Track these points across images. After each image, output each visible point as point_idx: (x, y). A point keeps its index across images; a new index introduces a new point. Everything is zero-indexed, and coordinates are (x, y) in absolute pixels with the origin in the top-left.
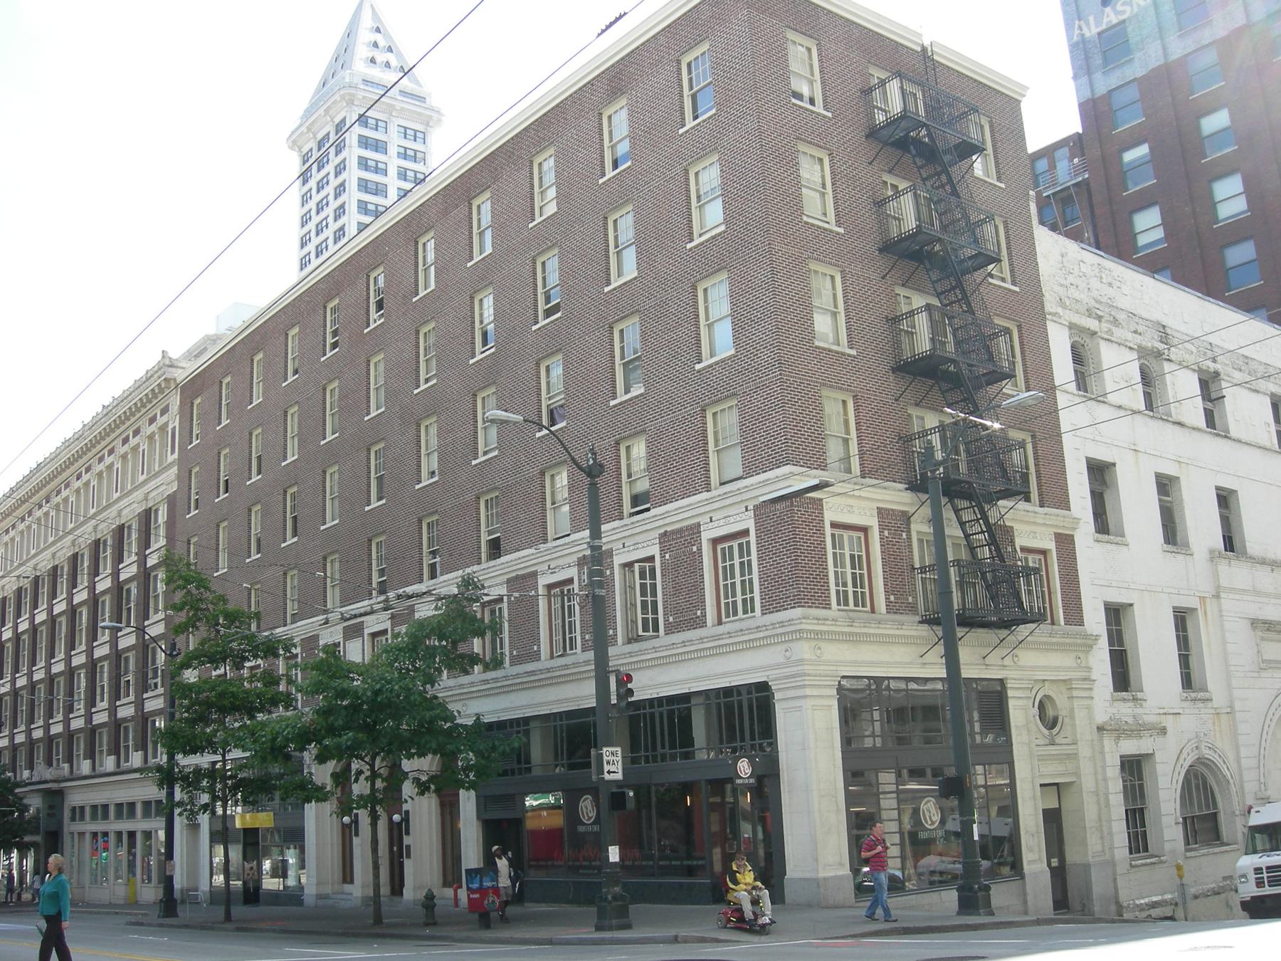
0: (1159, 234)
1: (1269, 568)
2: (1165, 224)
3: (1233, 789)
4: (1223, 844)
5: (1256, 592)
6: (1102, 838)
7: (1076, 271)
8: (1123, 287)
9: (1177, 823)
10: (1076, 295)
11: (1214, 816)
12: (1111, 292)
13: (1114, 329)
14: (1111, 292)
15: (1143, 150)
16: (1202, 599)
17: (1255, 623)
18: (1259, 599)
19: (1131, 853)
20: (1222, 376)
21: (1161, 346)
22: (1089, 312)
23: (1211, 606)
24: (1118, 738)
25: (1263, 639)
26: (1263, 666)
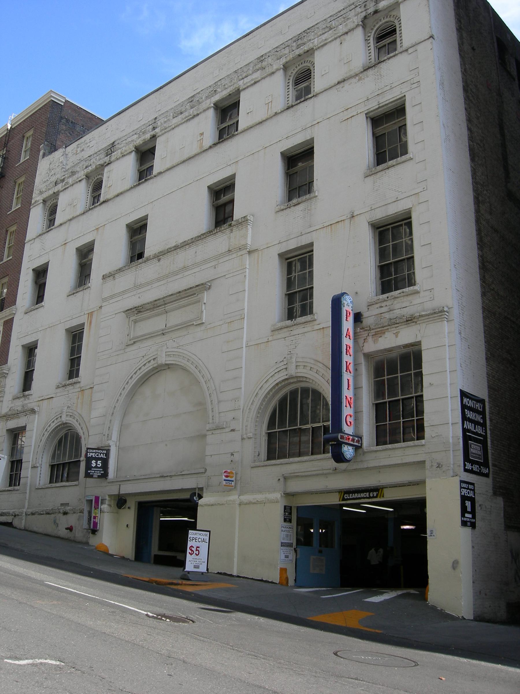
1: (155, 260)
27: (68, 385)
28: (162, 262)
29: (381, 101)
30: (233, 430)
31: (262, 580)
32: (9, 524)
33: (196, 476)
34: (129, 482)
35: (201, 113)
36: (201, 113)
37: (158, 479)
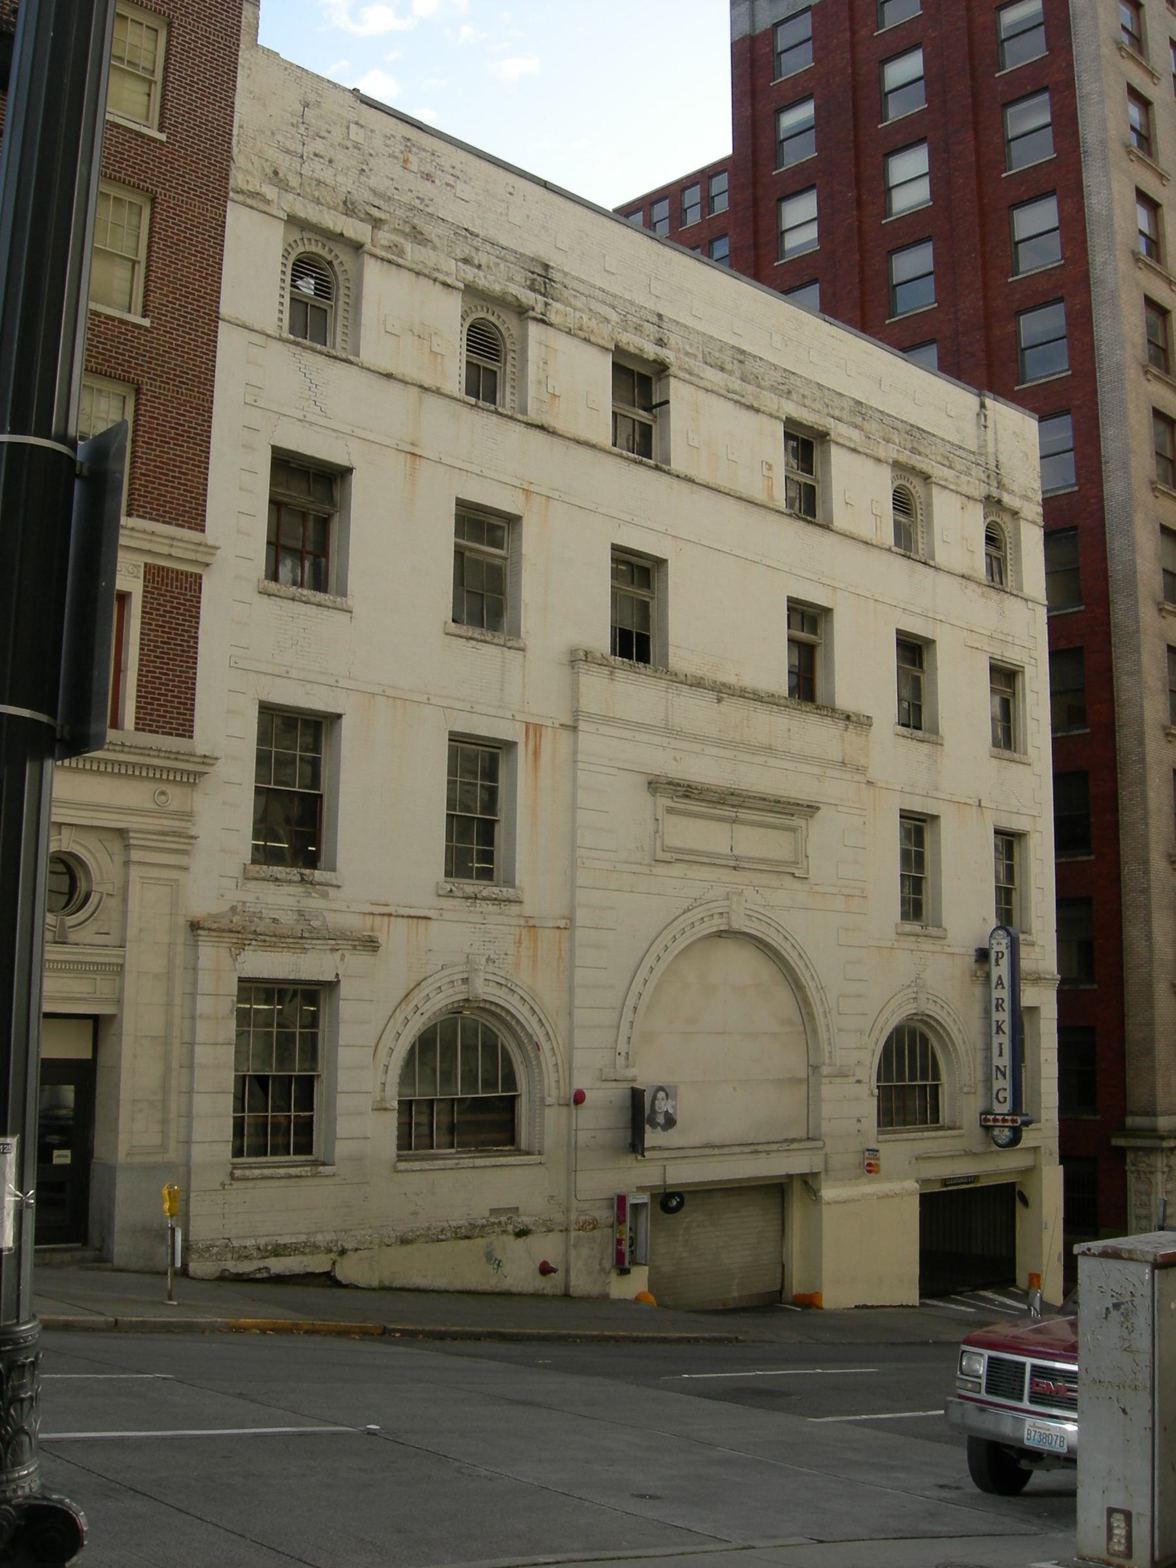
0: (810, 233)
1: (712, 696)
2: (820, 219)
3: (547, 1059)
4: (519, 1152)
5: (670, 731)
6: (164, 1122)
7: (338, 134)
8: (460, 185)
9: (381, 1109)
10: (327, 175)
11: (510, 1104)
12: (426, 189)
13: (408, 246)
14: (426, 189)
15: (805, 113)
16: (534, 730)
17: (654, 785)
18: (675, 744)
19: (238, 1152)
20: (673, 370)
21: (528, 297)
22: (349, 208)
23: (554, 745)
24: (242, 946)
25: (670, 811)
26: (660, 855)
27: (484, 899)
28: (724, 707)
29: (1006, 654)
30: (859, 1082)
31: (901, 1306)
32: (328, 1279)
33: (809, 1152)
34: (685, 1161)
35: (763, 412)
36: (763, 412)
37: (745, 1157)
